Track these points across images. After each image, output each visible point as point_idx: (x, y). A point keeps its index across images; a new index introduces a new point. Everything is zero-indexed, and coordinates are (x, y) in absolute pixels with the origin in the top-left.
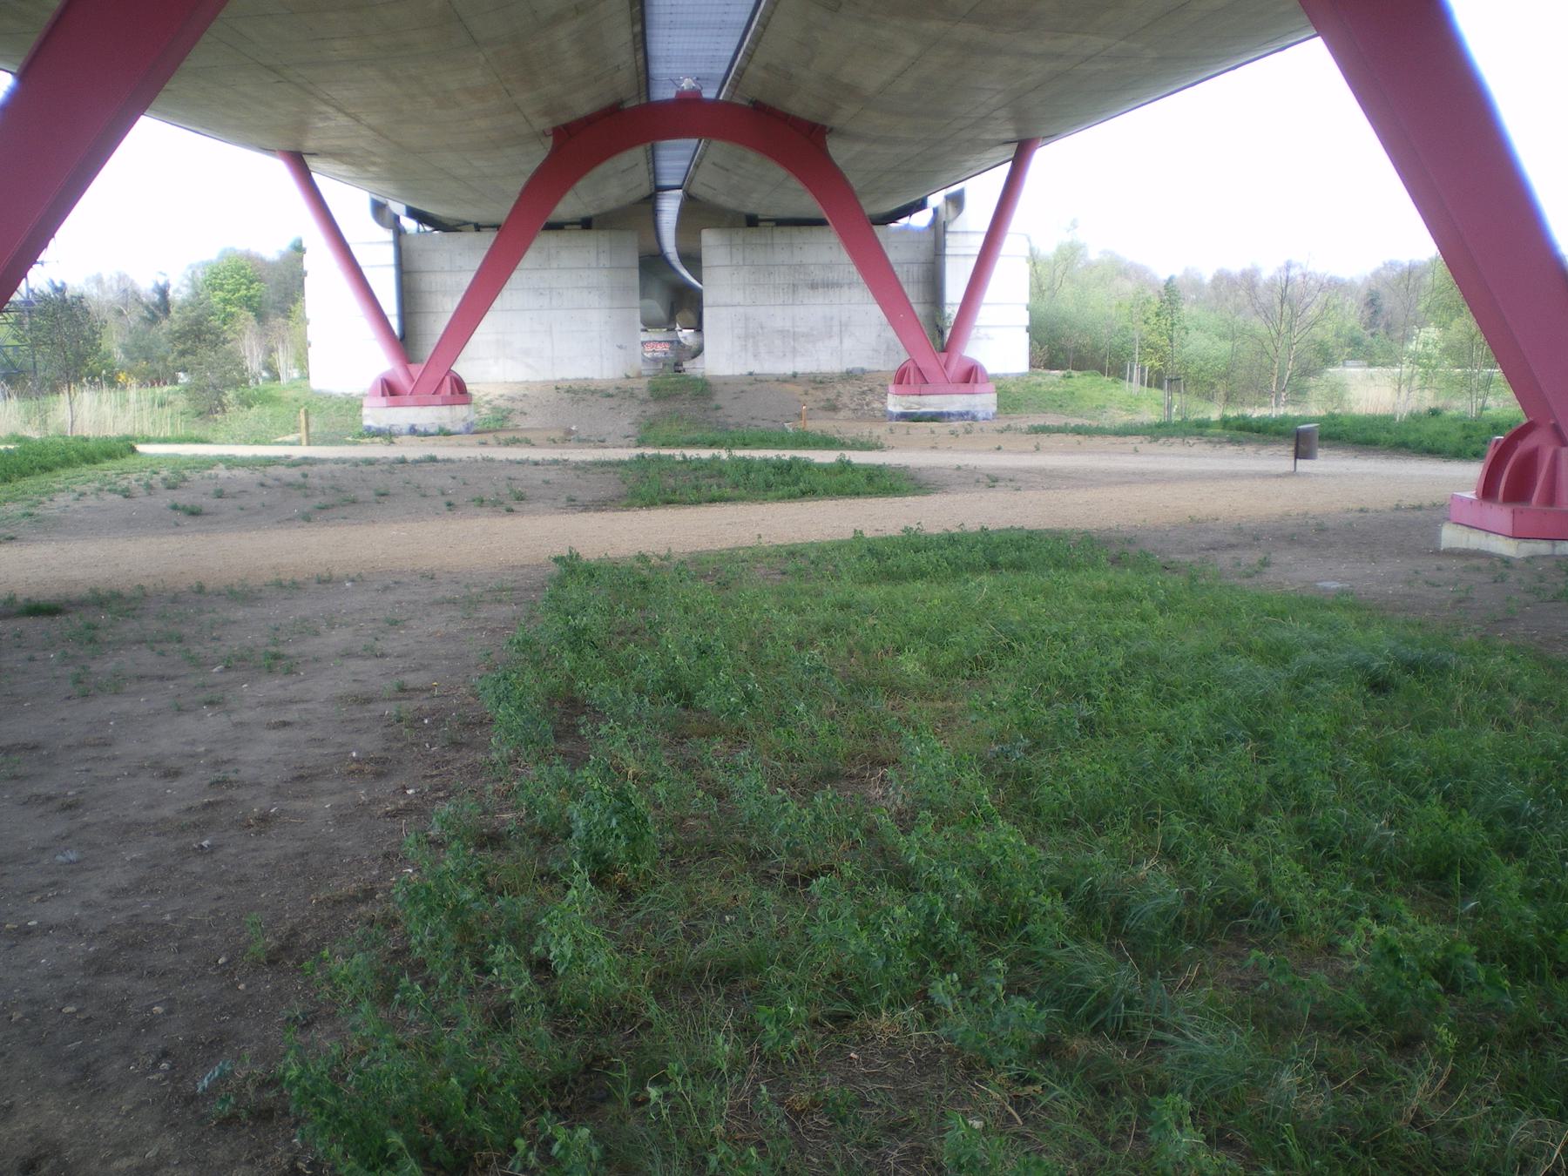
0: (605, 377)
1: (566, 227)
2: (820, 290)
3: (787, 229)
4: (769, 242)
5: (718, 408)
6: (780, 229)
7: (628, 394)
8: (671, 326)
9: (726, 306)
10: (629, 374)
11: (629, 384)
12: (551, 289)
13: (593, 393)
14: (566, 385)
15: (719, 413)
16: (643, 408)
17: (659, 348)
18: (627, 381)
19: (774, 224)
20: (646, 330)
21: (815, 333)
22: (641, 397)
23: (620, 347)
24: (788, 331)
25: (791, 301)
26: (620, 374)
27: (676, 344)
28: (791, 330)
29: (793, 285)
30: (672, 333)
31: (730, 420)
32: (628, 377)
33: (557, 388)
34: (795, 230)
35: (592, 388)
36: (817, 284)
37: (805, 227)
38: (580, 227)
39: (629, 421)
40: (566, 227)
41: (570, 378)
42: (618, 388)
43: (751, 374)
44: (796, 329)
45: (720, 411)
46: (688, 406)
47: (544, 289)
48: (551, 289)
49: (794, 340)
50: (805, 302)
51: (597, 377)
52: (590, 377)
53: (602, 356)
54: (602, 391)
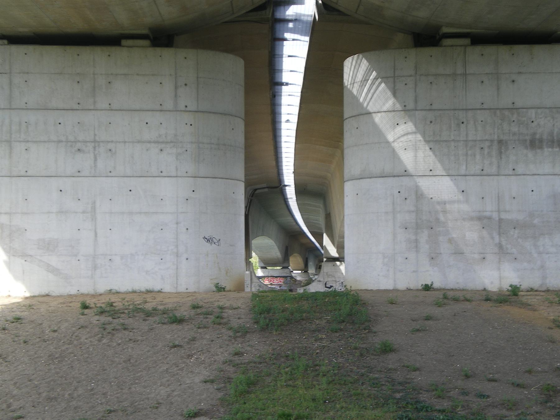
0: (182, 289)
1: (124, 42)
2: (547, 151)
3: (490, 50)
4: (460, 71)
5: (387, 349)
6: (478, 49)
7: (212, 318)
8: (285, 265)
9: (383, 176)
10: (223, 284)
11: (223, 300)
12: (96, 142)
13: (148, 314)
14: (102, 302)
15: (391, 361)
16: (238, 346)
17: (276, 281)
18: (218, 296)
19: (467, 41)
20: (265, 268)
21: (536, 221)
22: (235, 323)
23: (209, 240)
24: (490, 218)
25: (494, 170)
26: (206, 284)
27: (289, 278)
28: (495, 215)
29: (500, 142)
30: (286, 270)
31: (419, 379)
32: (220, 289)
33: (85, 307)
34: (503, 51)
35: (149, 307)
36: (541, 141)
37: (521, 47)
38: (146, 42)
39: (205, 373)
40: (124, 42)
41: (123, 289)
42: (195, 307)
43: (427, 288)
44: (504, 216)
45: (392, 356)
46: (325, 343)
47: (85, 142)
48: (96, 142)
49: (499, 234)
50: (520, 169)
51: (168, 288)
52: (157, 288)
53: (177, 255)
54: (164, 312)
